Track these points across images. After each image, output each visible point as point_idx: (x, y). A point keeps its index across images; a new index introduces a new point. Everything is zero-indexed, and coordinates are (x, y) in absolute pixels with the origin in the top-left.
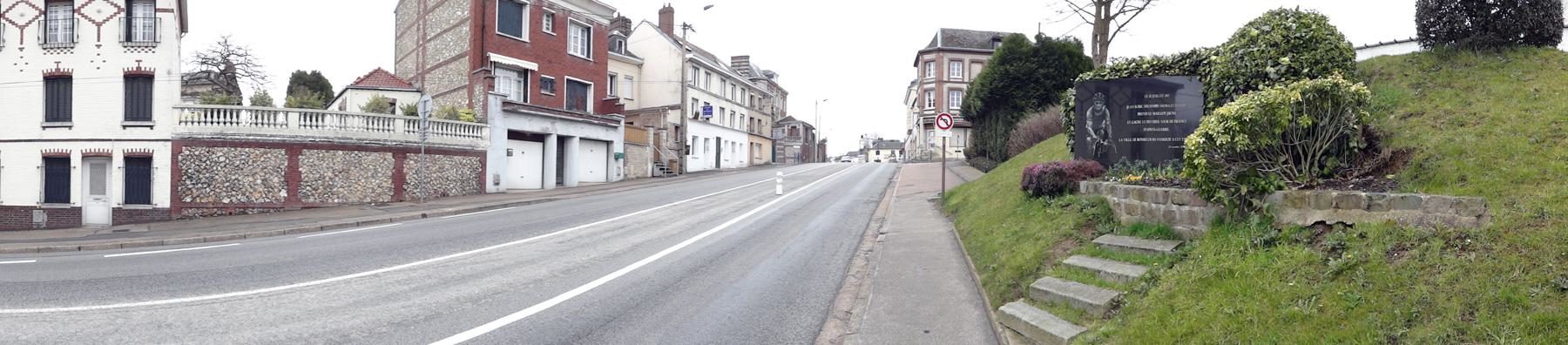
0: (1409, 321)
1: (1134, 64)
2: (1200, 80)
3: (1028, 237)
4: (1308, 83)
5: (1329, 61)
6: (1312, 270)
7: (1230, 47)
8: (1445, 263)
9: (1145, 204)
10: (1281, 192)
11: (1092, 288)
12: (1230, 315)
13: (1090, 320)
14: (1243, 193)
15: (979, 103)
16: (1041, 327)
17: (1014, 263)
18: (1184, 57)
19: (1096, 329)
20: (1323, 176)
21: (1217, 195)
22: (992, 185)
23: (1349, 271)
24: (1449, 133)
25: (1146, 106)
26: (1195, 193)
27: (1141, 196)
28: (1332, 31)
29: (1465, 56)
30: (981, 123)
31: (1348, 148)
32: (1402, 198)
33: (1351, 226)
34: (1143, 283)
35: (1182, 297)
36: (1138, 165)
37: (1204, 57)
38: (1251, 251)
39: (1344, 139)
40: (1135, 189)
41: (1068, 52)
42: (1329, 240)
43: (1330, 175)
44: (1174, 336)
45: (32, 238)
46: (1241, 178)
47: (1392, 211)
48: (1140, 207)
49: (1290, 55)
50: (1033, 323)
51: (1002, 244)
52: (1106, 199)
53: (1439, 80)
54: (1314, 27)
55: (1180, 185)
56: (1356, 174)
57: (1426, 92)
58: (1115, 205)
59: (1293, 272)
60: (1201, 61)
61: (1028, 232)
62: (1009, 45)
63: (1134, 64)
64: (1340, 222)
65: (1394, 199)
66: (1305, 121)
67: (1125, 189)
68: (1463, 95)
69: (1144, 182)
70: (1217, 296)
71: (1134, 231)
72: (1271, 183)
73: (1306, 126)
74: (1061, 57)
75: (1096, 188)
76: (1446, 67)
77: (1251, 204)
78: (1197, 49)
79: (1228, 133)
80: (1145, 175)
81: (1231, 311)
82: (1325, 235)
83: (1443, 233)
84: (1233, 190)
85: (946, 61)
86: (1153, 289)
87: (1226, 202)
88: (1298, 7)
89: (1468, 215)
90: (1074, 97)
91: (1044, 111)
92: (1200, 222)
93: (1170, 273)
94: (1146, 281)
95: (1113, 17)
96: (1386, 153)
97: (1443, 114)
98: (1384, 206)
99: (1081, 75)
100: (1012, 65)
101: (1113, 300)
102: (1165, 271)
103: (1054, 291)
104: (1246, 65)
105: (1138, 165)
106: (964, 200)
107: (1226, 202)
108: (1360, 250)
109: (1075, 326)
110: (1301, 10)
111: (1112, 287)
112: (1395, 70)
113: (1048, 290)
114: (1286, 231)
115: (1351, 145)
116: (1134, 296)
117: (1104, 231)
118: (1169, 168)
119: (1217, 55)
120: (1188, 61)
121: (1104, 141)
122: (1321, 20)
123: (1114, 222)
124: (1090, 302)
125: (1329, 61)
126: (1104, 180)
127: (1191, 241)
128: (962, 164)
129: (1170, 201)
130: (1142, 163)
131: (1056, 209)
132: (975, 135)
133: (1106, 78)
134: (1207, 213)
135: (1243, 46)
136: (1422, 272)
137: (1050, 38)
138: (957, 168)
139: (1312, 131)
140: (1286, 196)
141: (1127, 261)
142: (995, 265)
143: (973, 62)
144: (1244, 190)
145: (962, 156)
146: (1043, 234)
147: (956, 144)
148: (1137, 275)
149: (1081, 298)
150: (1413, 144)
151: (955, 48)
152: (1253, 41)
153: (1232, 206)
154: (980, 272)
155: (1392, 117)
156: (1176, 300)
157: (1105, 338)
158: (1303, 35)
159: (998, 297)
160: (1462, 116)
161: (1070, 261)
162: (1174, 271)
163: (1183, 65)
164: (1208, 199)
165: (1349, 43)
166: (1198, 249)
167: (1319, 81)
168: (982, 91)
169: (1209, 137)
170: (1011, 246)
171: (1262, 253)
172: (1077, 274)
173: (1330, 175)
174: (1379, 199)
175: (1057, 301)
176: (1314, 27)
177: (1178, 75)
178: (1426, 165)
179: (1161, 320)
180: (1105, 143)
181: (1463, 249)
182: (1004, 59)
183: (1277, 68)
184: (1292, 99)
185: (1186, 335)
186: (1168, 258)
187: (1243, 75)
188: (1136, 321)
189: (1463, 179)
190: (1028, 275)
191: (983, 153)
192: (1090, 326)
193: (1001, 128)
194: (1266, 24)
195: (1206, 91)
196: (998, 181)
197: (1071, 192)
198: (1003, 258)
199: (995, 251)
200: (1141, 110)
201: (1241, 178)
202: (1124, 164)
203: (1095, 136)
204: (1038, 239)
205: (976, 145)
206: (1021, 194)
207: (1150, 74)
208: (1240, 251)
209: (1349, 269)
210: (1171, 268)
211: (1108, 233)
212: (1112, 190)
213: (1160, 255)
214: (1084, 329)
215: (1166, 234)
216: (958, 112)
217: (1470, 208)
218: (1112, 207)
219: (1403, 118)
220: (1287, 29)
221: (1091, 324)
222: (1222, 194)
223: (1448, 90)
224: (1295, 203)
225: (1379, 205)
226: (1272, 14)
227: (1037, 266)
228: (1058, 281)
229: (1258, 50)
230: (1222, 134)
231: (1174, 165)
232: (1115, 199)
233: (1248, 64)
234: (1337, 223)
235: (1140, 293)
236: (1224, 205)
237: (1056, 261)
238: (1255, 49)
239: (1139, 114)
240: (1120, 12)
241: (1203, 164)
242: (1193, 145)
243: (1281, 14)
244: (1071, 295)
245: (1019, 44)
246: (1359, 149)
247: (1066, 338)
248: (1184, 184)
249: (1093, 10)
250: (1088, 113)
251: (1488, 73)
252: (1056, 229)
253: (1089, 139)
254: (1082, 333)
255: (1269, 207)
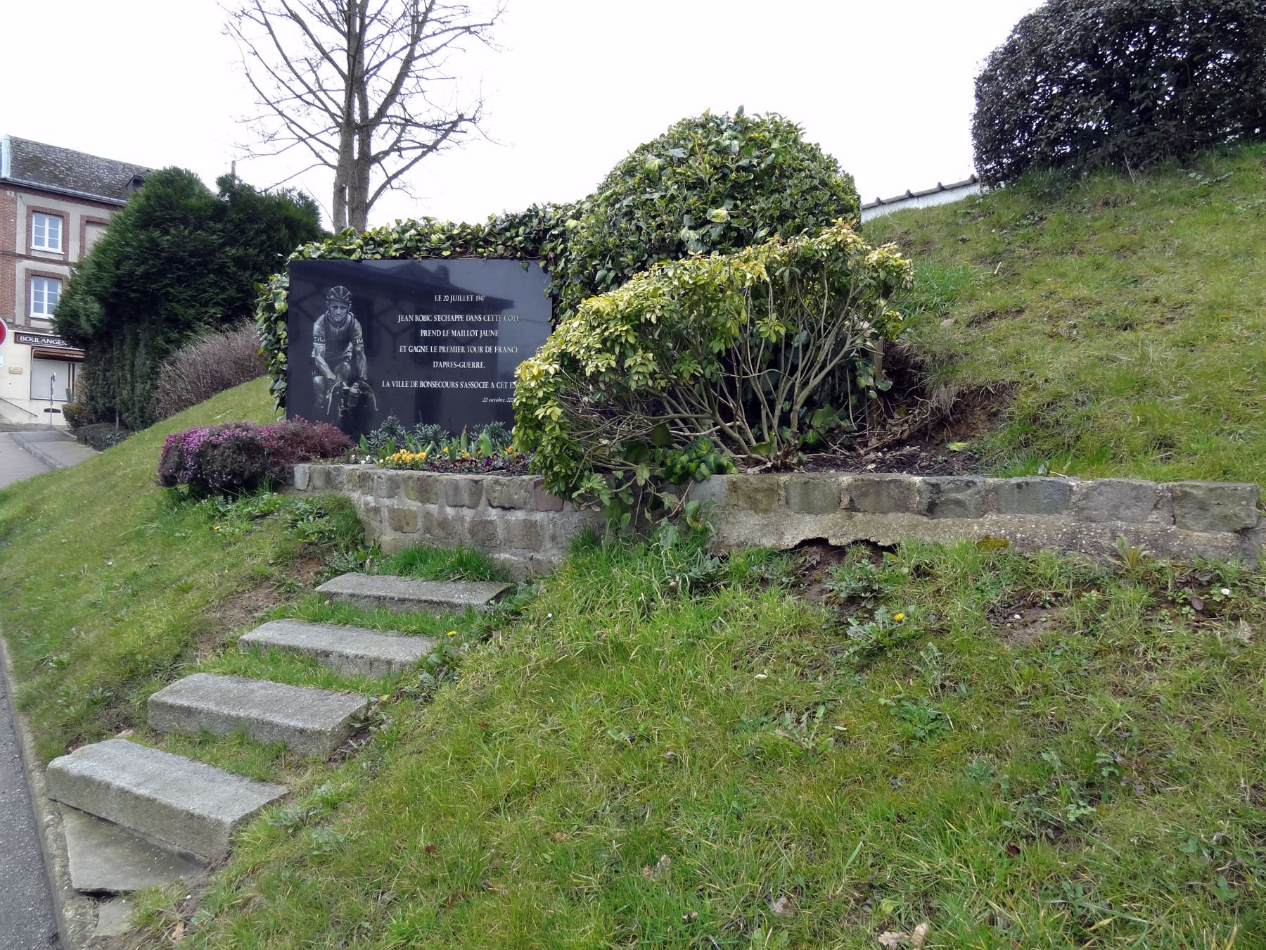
0: (1090, 785)
1: (413, 232)
2: (545, 269)
3: (160, 587)
4: (776, 249)
5: (810, 212)
6: (807, 644)
7: (609, 196)
8: (1162, 641)
9: (433, 508)
10: (724, 477)
11: (307, 694)
12: (621, 747)
13: (299, 767)
14: (641, 482)
15: (95, 307)
16: (164, 799)
17: (114, 649)
18: (514, 223)
19: (309, 788)
20: (805, 448)
21: (586, 485)
22: (104, 477)
23: (899, 651)
24: (1098, 346)
25: (439, 318)
26: (537, 484)
27: (424, 491)
28: (813, 153)
29: (1099, 185)
30: (104, 351)
31: (855, 388)
32: (1019, 486)
33: (892, 549)
34: (424, 676)
35: (508, 705)
36: (420, 434)
37: (553, 222)
38: (663, 603)
39: (849, 367)
40: (410, 478)
41: (286, 217)
42: (842, 580)
43: (820, 446)
44: (489, 796)
45: (23, 296)
46: (635, 449)
47: (992, 517)
48: (420, 515)
49: (729, 203)
50: (143, 791)
51: (94, 605)
52: (348, 500)
53: (1046, 241)
54: (775, 145)
55: (508, 469)
56: (874, 442)
57: (1018, 267)
58: (368, 510)
59: (762, 650)
60: (546, 231)
61: (165, 576)
62: (161, 190)
63: (413, 232)
64: (862, 541)
65: (996, 489)
66: (772, 327)
67: (391, 479)
68: (1113, 263)
69: (432, 466)
70: (588, 704)
71: (409, 564)
72: (701, 460)
73: (774, 339)
74: (271, 227)
75: (328, 478)
76: (1054, 217)
77: (658, 503)
78: (540, 207)
79: (611, 351)
80: (433, 450)
81: (624, 736)
82: (830, 569)
83: (1140, 569)
84: (620, 474)
85: (21, 211)
86: (445, 688)
87: (605, 499)
88: (741, 110)
89: (1211, 527)
90: (284, 293)
91: (235, 330)
92: (548, 544)
93: (483, 651)
94: (430, 670)
95: (377, 159)
96: (943, 396)
97: (1069, 309)
98: (972, 508)
99: (300, 248)
100: (167, 233)
101: (354, 717)
102: (473, 648)
103: (212, 707)
104: (639, 229)
105: (420, 434)
106: (29, 510)
107: (605, 499)
108: (920, 604)
109: (257, 786)
110: (748, 114)
111: (351, 687)
112: (934, 233)
113: (194, 705)
114: (737, 560)
115: (864, 382)
116: (403, 704)
117: (343, 565)
118: (484, 436)
119: (578, 219)
120: (521, 230)
121: (350, 385)
122: (788, 133)
123: (366, 548)
124: (300, 725)
125: (810, 212)
126: (348, 462)
127: (529, 583)
128: (60, 436)
129: (484, 500)
130: (429, 430)
131: (238, 523)
132: (89, 376)
133: (353, 257)
134: (563, 525)
135: (633, 191)
136: (1098, 664)
137: (250, 188)
138: (38, 445)
139: (777, 354)
140: (734, 487)
141: (392, 628)
142: (65, 657)
143: (35, 211)
144: (643, 474)
145: (60, 421)
146: (201, 577)
147: (47, 395)
148: (410, 658)
149: (278, 719)
150: (1009, 375)
151: (44, 185)
152: (652, 180)
153: (618, 511)
154: (23, 674)
155: (946, 323)
156: (495, 711)
157: (327, 812)
158: (755, 162)
159: (59, 733)
160: (1122, 307)
161: (261, 634)
162: (492, 647)
163: (512, 238)
164: (566, 495)
165: (847, 175)
166: (544, 598)
167: (801, 242)
168: (99, 279)
169: (570, 363)
170: (115, 609)
171: (687, 605)
172: (275, 661)
173: (820, 446)
174: (958, 490)
175: (219, 729)
176: (775, 145)
177: (501, 257)
178: (1050, 417)
179: (462, 759)
180: (354, 390)
181: (1209, 612)
182: (146, 219)
183: (702, 231)
184: (749, 276)
185: (517, 794)
186: (479, 620)
187: (633, 247)
188: (402, 764)
189: (1165, 443)
190: (148, 674)
191: (108, 416)
192: (299, 782)
193: (142, 360)
194: (676, 146)
195: (555, 292)
196: (118, 468)
197: (276, 486)
198: (88, 638)
199: (71, 624)
200: (428, 326)
201: (635, 449)
202: (392, 432)
203: (330, 375)
204: (184, 590)
205: (92, 398)
206: (161, 493)
207: (446, 253)
208: (639, 604)
209: (899, 644)
210: (486, 640)
211: (353, 570)
212: (363, 481)
213: (461, 613)
214: (282, 790)
215: (477, 569)
216: (47, 325)
217: (1217, 510)
218: (361, 515)
219: (975, 322)
220: (723, 151)
221: (299, 775)
222: (596, 482)
223: (1071, 259)
224: (754, 501)
225: (958, 503)
226: (689, 125)
227: (177, 650)
228: (227, 683)
229: (662, 197)
230: (599, 351)
231: (494, 435)
232: (370, 498)
233: (642, 224)
234: (854, 543)
235: (416, 697)
236: (600, 504)
237: (227, 637)
238: (656, 196)
239: (424, 333)
240: (392, 149)
241: (554, 418)
242: (533, 377)
243: (708, 125)
244: (254, 713)
245: (183, 190)
246: (879, 392)
247: (228, 820)
248: (514, 467)
249: (336, 141)
250: (316, 326)
251: (1170, 211)
252: (233, 566)
253: (317, 379)
254: (271, 803)
255: (698, 509)
